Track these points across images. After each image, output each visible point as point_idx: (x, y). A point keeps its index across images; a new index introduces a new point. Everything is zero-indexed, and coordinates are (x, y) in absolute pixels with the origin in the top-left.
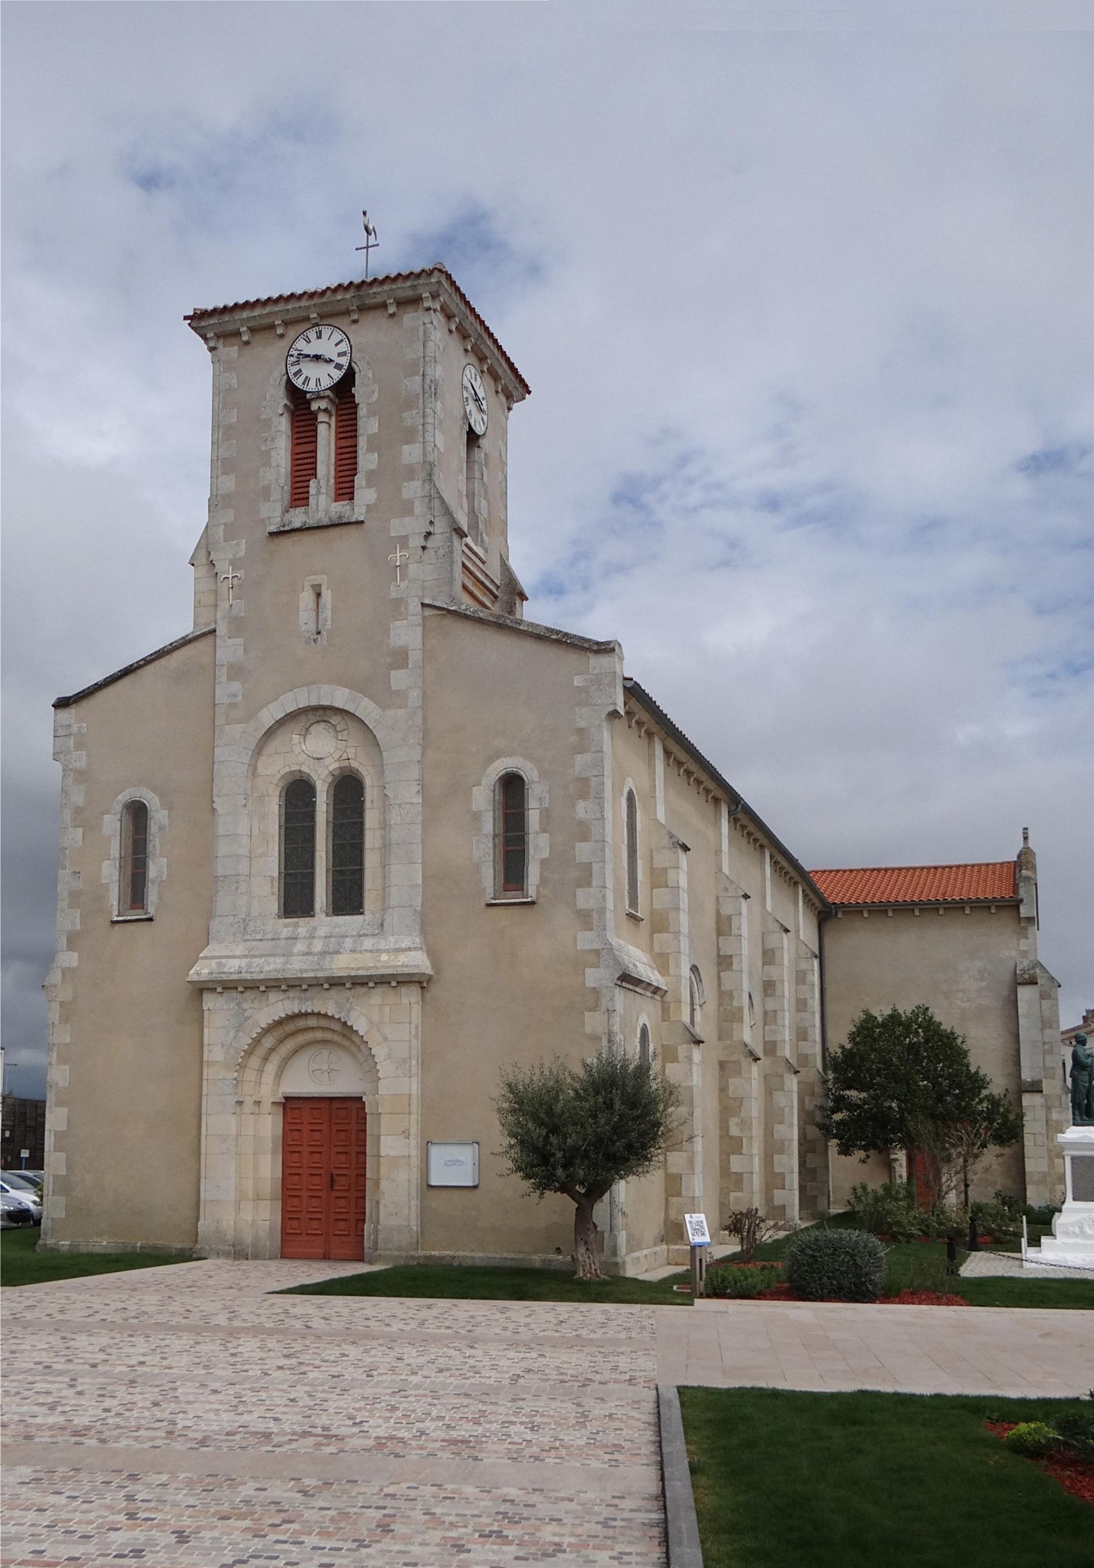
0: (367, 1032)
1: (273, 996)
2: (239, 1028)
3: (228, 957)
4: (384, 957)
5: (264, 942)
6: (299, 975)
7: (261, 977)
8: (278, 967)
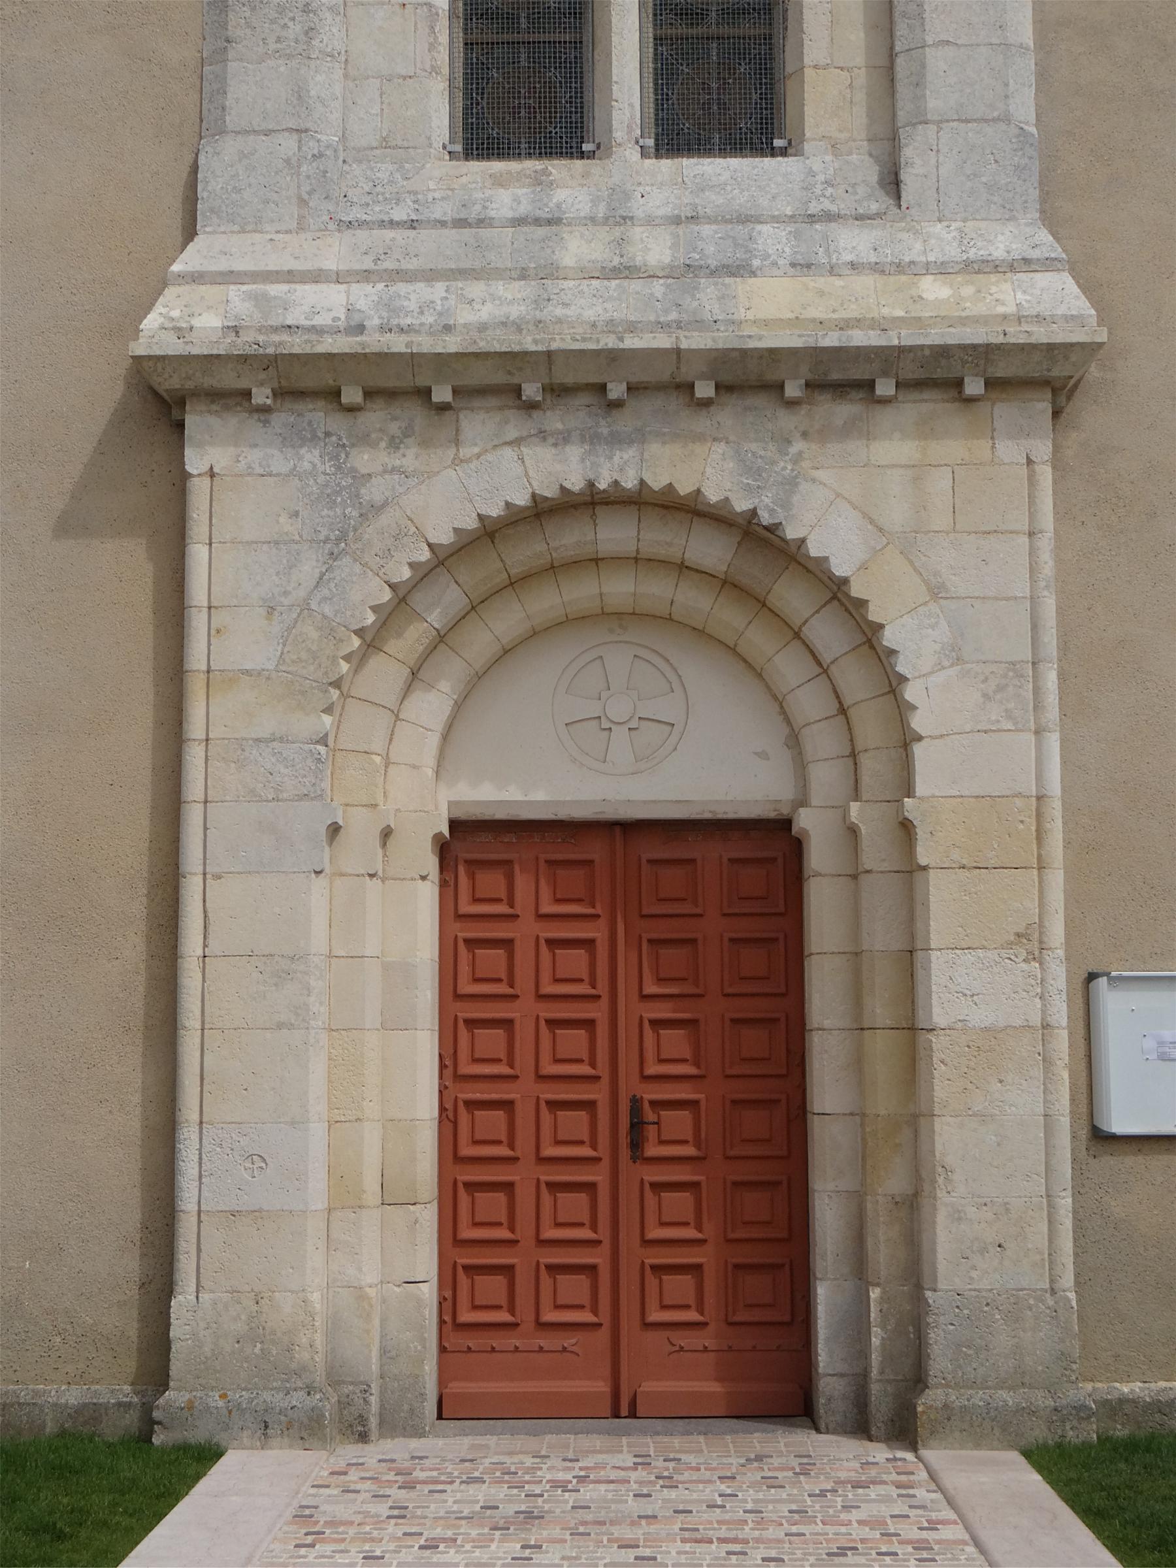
0: (864, 567)
1: (478, 425)
2: (339, 544)
3: (290, 277)
4: (934, 290)
5: (424, 233)
6: (610, 342)
7: (452, 344)
8: (515, 312)
